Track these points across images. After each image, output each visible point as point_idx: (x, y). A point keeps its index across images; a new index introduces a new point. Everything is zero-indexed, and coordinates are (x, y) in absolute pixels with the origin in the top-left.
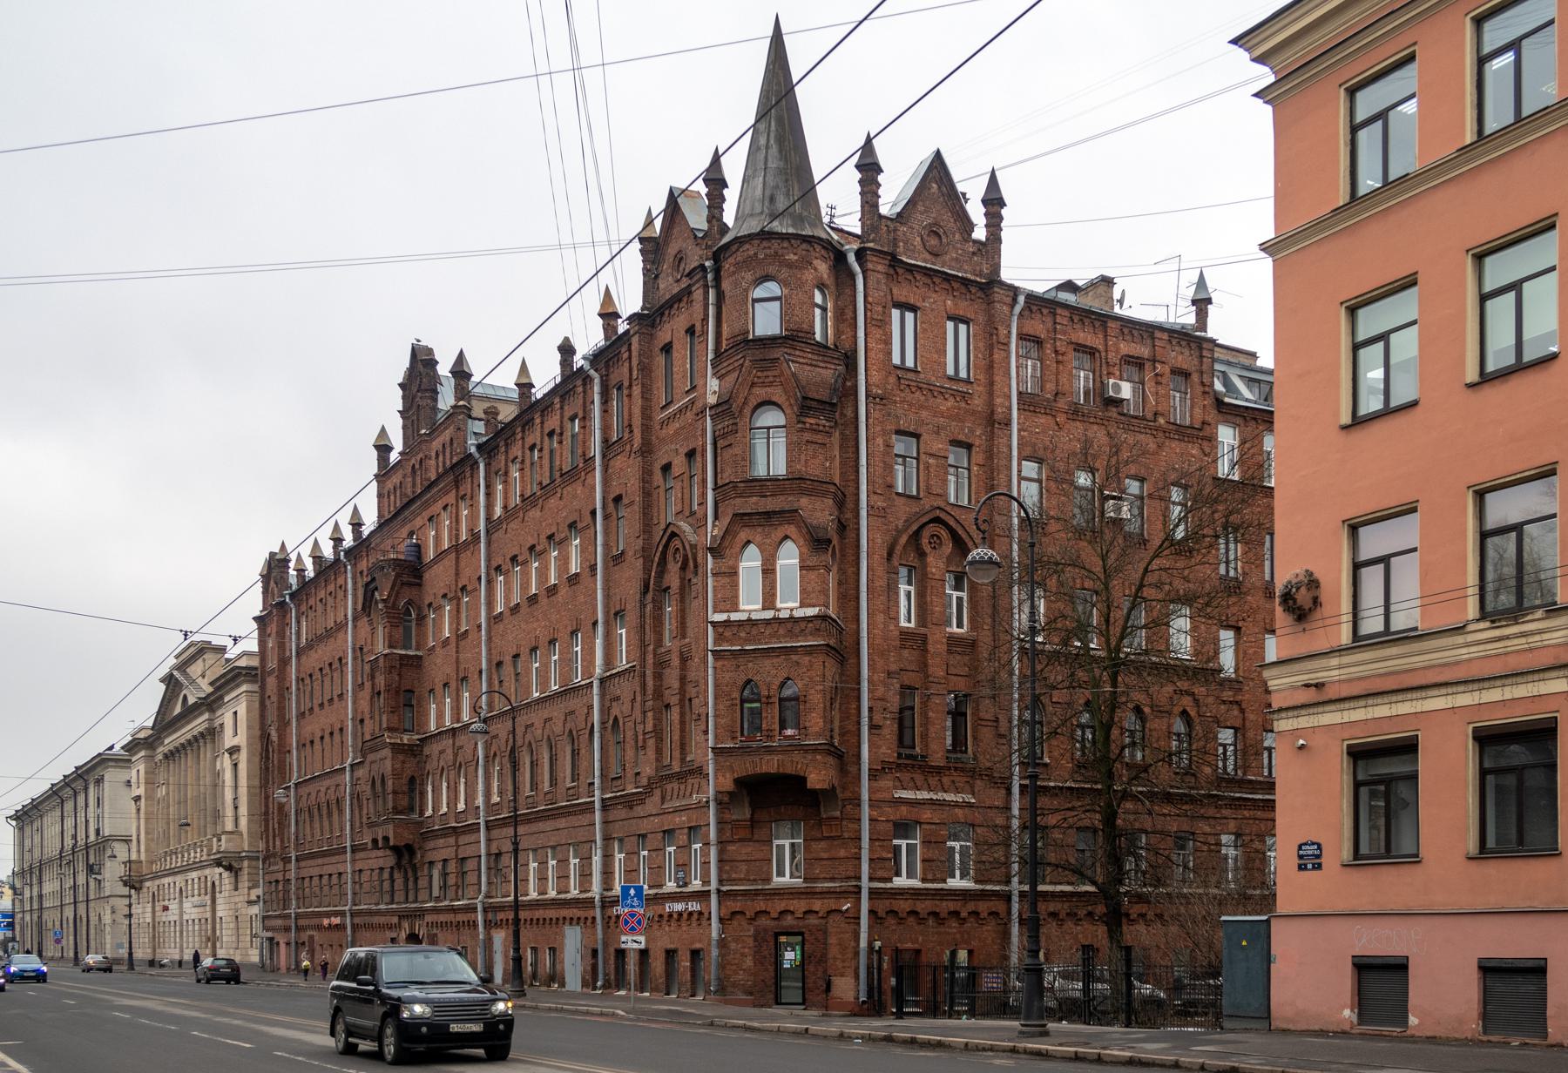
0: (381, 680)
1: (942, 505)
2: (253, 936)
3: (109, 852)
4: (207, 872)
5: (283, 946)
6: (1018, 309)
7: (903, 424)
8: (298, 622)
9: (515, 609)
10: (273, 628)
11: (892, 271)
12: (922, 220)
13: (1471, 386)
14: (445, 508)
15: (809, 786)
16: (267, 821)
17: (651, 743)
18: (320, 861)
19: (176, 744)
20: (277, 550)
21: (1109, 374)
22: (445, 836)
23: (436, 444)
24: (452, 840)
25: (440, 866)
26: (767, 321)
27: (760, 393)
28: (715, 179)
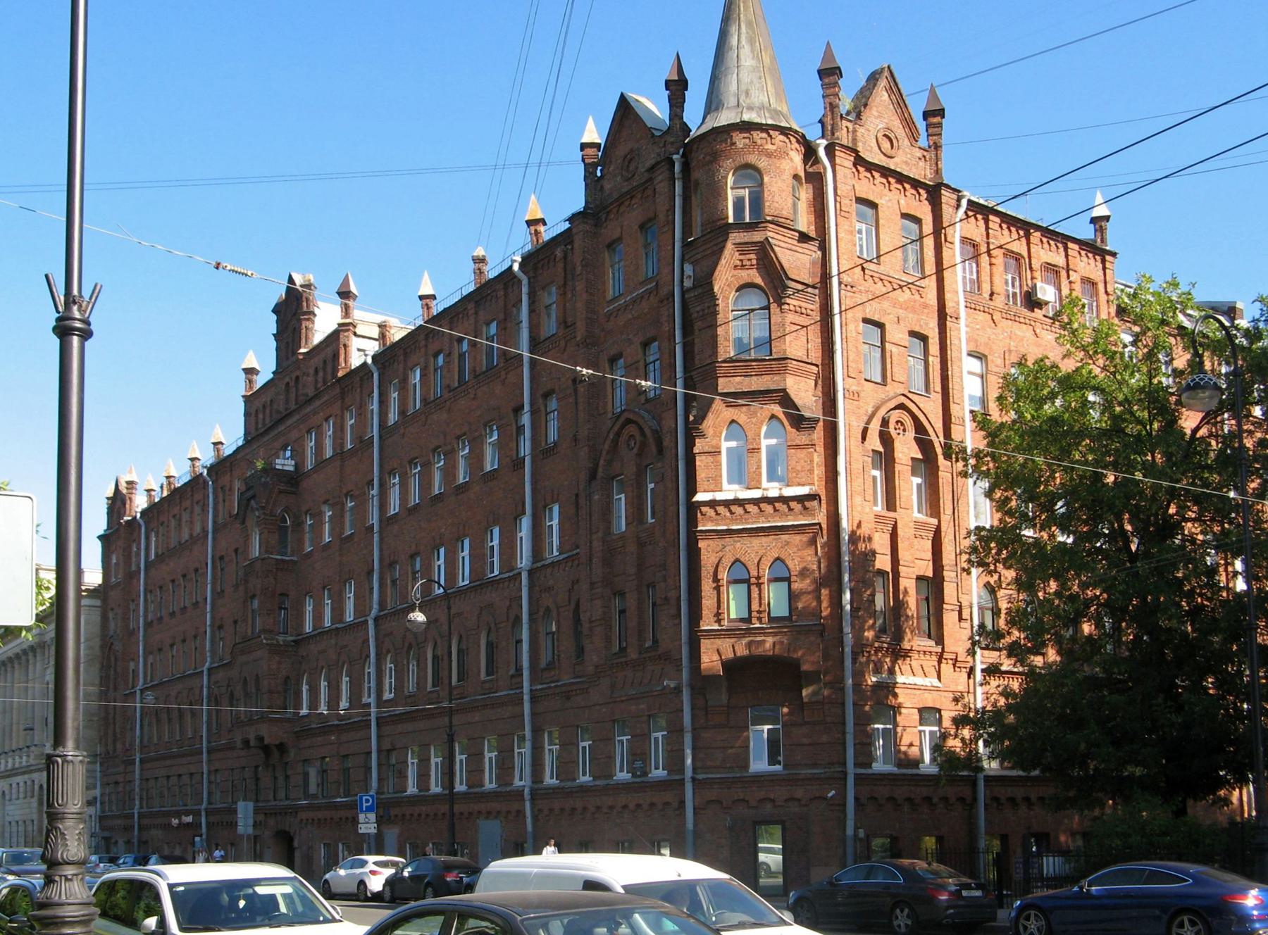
18: (168, 762)
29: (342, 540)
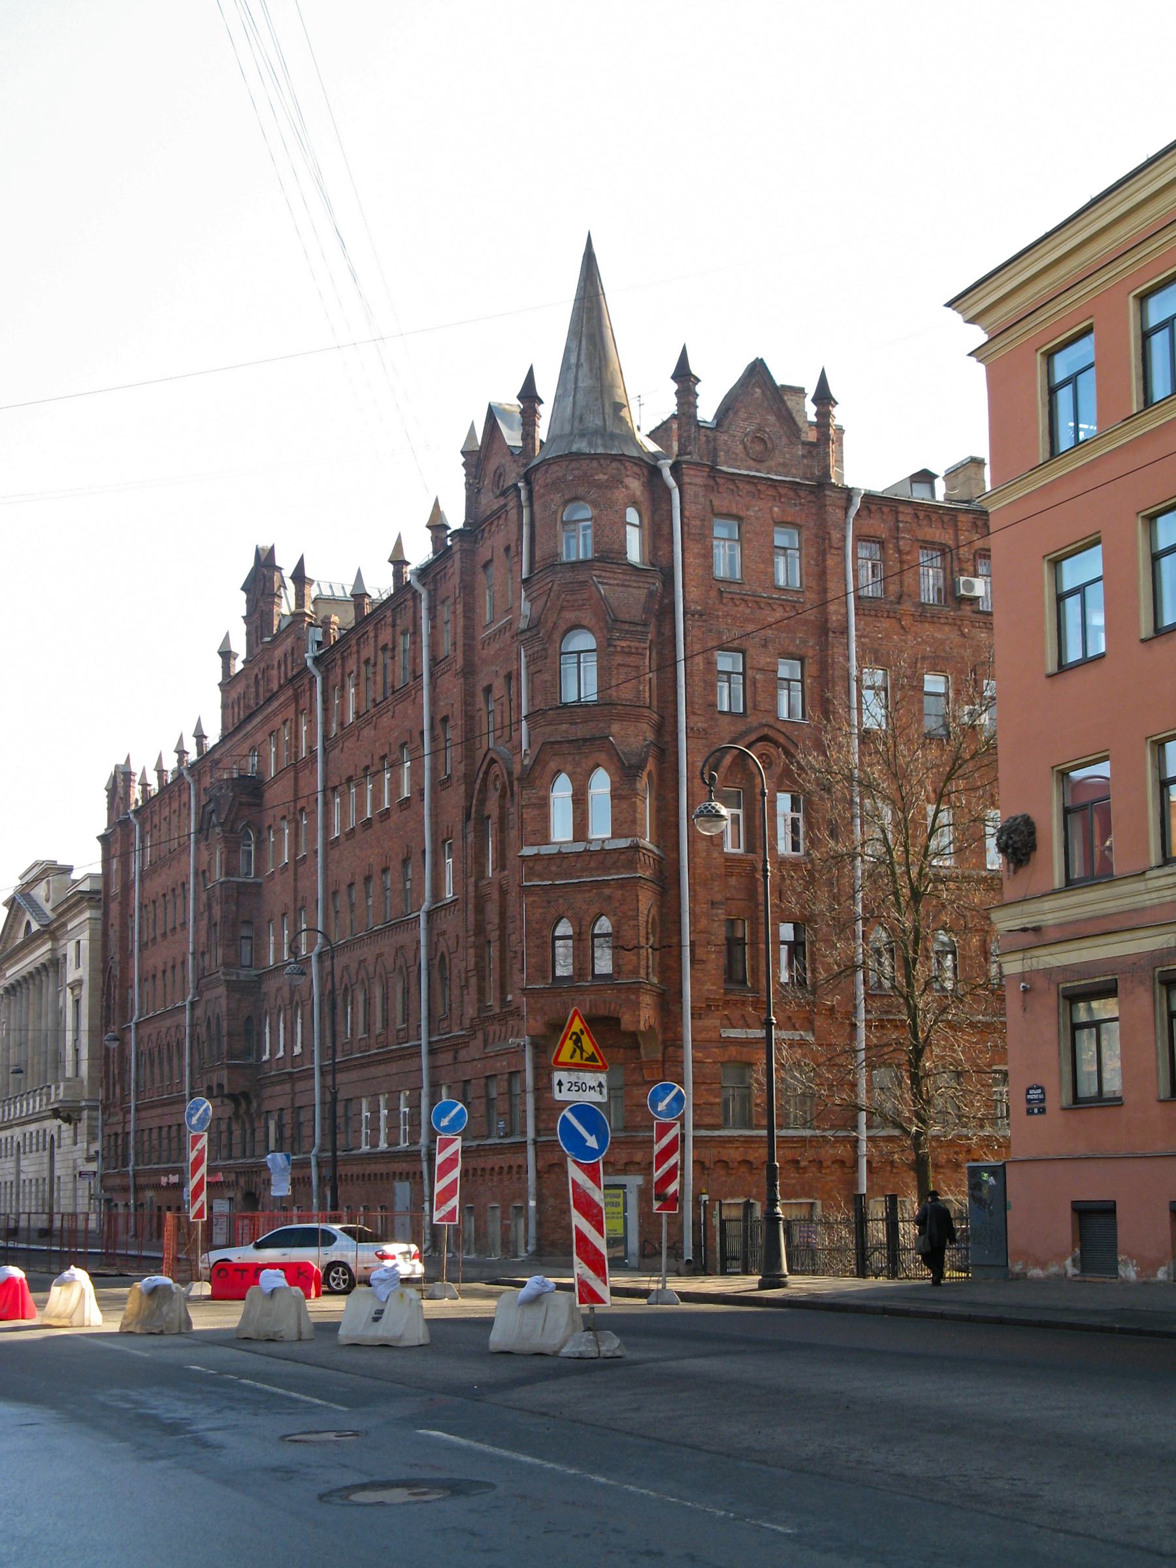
0: (217, 911)
1: (771, 721)
6: (853, 512)
11: (711, 482)
12: (743, 426)
13: (1049, 676)
14: (284, 723)
15: (623, 1027)
16: (107, 1064)
17: (473, 981)
18: (160, 1111)
19: (18, 977)
21: (962, 572)
22: (281, 1082)
23: (278, 653)
24: (288, 1087)
27: (570, 616)
28: (529, 395)
29: (296, 862)
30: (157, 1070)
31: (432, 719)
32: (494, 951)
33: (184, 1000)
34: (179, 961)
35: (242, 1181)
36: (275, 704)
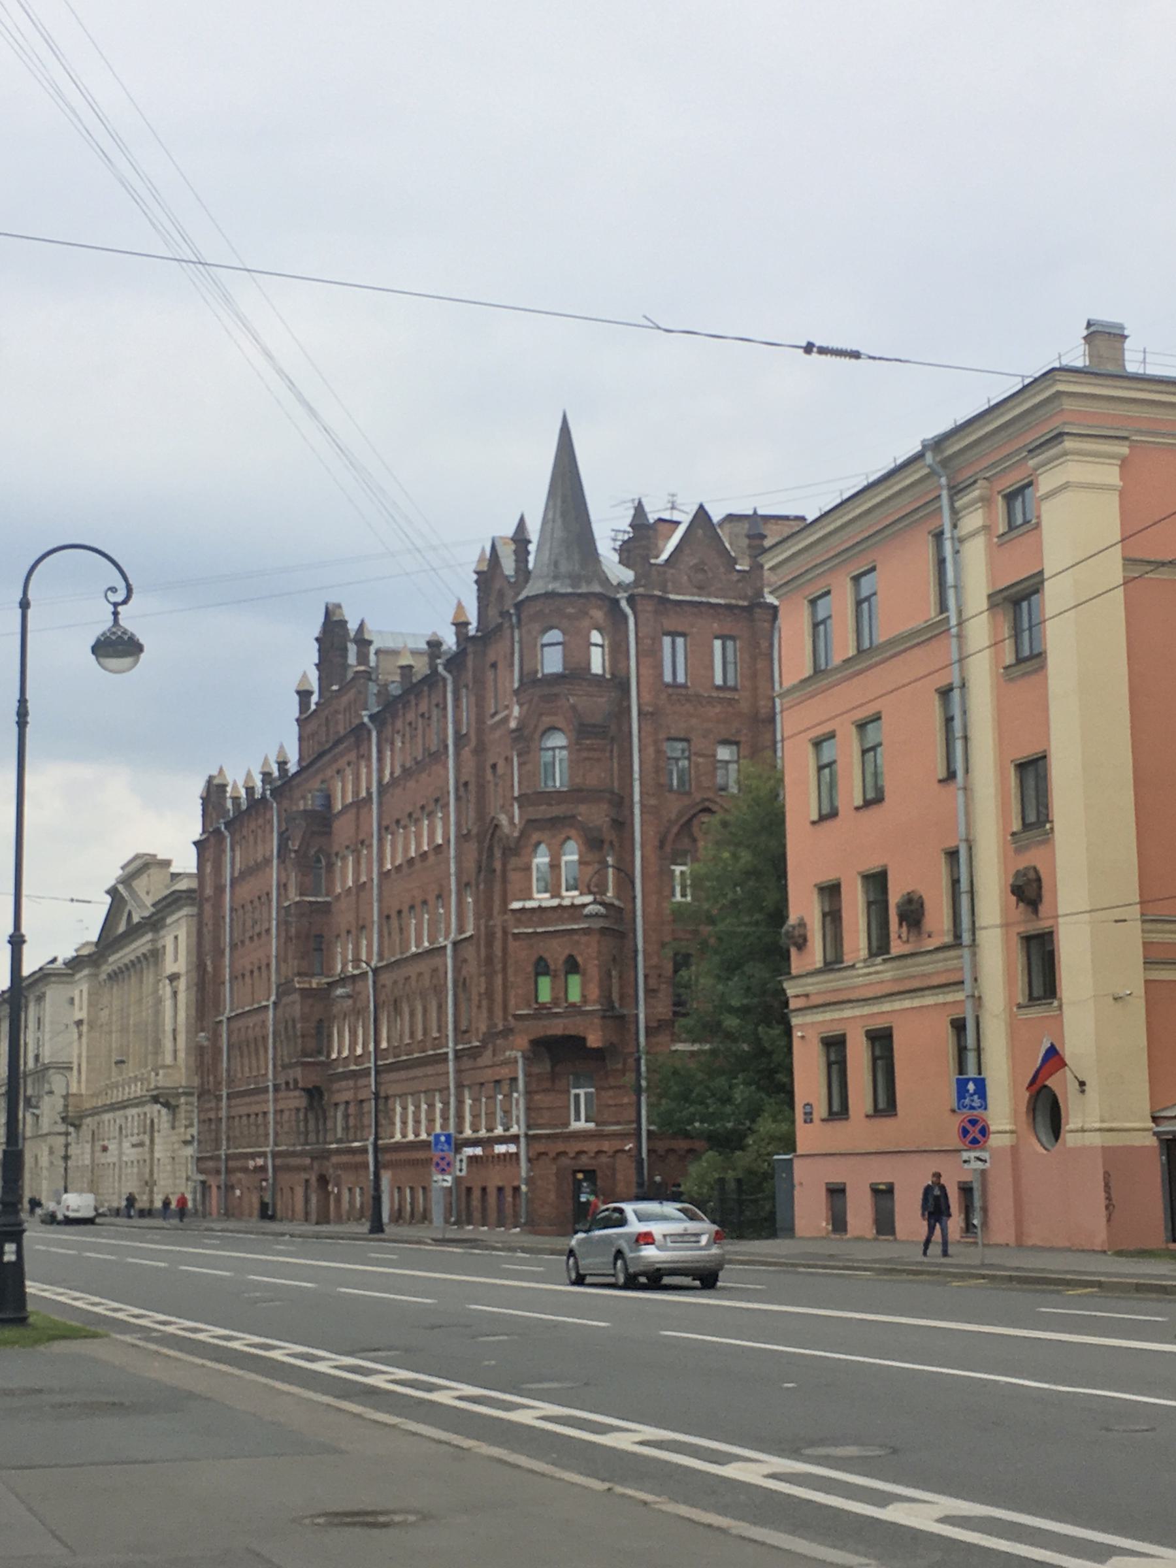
2: (188, 1179)
3: (47, 1087)
4: (147, 1108)
5: (214, 1190)
7: (673, 733)
8: (233, 850)
9: (398, 868)
10: (209, 854)
17: (484, 1003)
18: (247, 1100)
20: (215, 773)
24: (351, 1083)
25: (342, 1108)
26: (552, 662)
27: (547, 721)
30: (246, 1061)
31: (457, 781)
32: (499, 980)
33: (268, 1000)
34: (264, 963)
35: (316, 1165)
36: (342, 747)
